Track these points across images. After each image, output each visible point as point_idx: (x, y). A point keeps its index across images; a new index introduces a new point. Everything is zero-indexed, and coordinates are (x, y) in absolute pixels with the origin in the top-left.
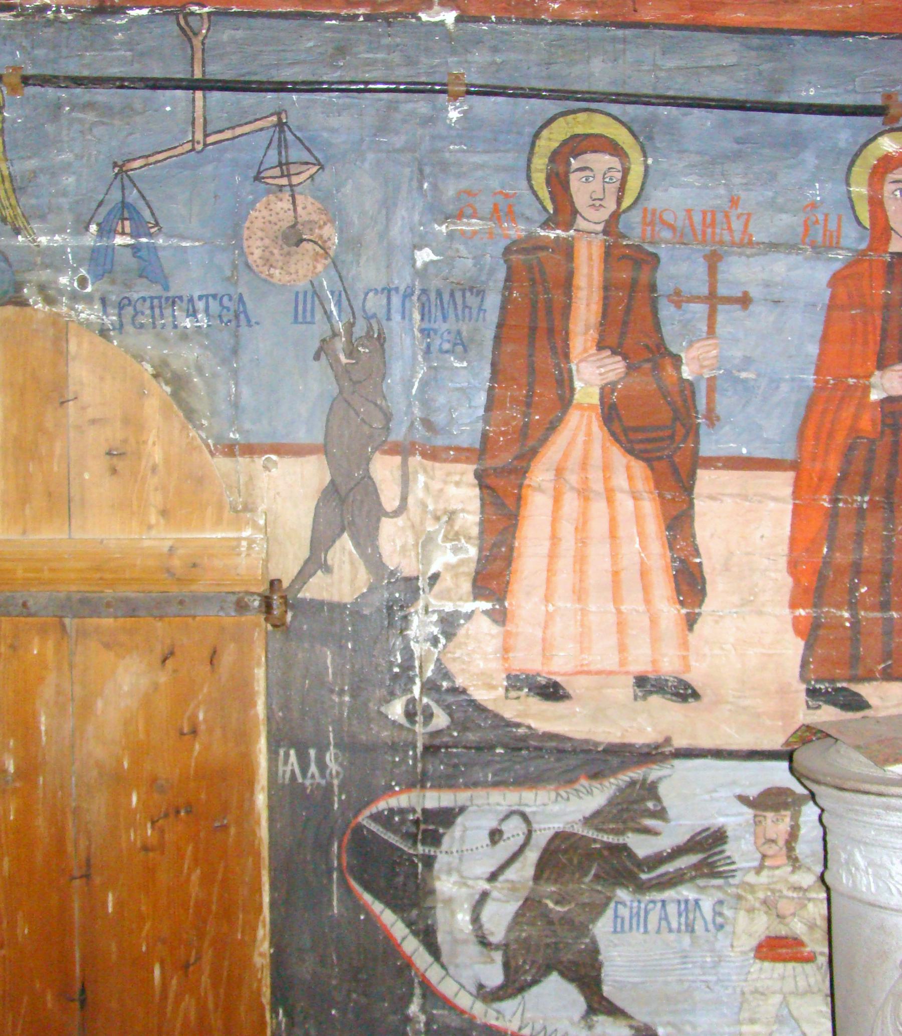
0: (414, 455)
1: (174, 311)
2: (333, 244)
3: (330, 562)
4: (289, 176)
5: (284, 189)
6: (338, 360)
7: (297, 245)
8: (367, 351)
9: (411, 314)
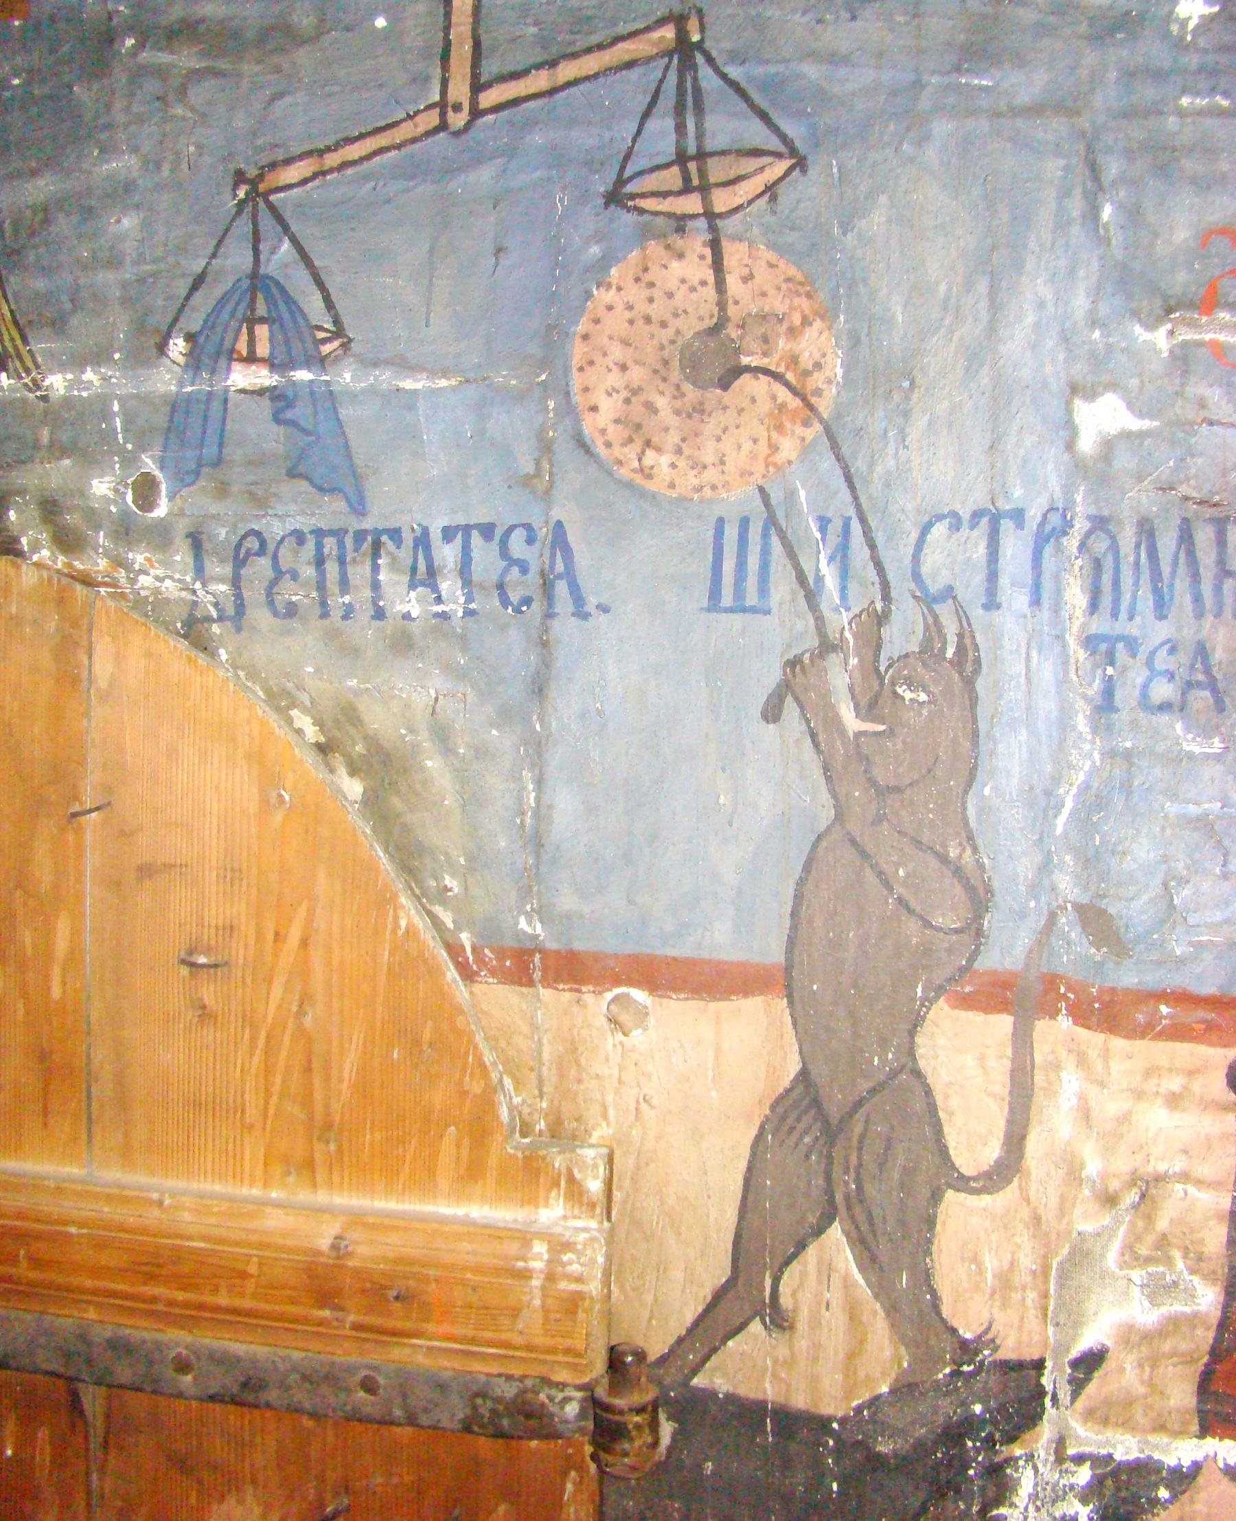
0: (1054, 1014)
1: (376, 569)
2: (829, 382)
3: (785, 1301)
4: (704, 189)
5: (690, 224)
6: (835, 722)
7: (725, 384)
8: (923, 697)
9: (1059, 592)
